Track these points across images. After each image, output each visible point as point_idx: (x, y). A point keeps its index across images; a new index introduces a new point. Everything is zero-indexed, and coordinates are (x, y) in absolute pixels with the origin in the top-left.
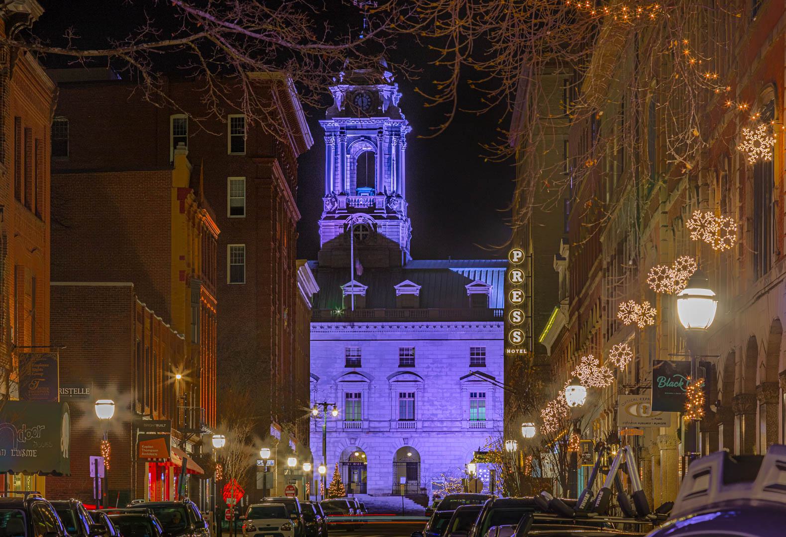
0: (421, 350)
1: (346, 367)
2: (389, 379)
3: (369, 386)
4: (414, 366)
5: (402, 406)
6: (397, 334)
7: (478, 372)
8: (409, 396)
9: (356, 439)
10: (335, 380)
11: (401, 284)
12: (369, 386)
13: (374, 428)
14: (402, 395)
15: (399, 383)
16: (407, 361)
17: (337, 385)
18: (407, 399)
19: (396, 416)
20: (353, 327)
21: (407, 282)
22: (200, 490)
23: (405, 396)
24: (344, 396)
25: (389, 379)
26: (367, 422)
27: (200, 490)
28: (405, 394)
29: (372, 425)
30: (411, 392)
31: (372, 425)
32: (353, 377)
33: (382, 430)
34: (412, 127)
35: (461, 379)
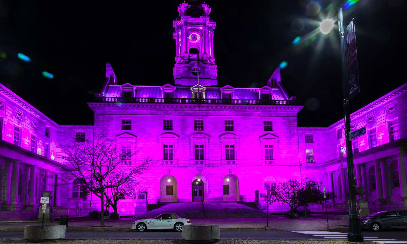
0: (238, 121)
1: (122, 129)
2: (220, 136)
3: (209, 140)
4: (233, 130)
5: (266, 151)
6: (224, 112)
7: (269, 133)
8: (231, 147)
9: (201, 170)
10: (189, 137)
11: (224, 87)
12: (209, 140)
13: (212, 164)
14: (227, 146)
15: (226, 139)
16: (229, 127)
17: (190, 140)
18: (269, 148)
19: (224, 157)
20: (199, 107)
21: (228, 86)
22: (200, 226)
23: (198, 147)
24: (194, 146)
25: (220, 136)
26: (208, 161)
27: (200, 226)
28: (267, 146)
29: (211, 162)
30: (232, 144)
31: (211, 162)
32: (199, 136)
33: (216, 165)
34: (172, 23)
35: (260, 137)
